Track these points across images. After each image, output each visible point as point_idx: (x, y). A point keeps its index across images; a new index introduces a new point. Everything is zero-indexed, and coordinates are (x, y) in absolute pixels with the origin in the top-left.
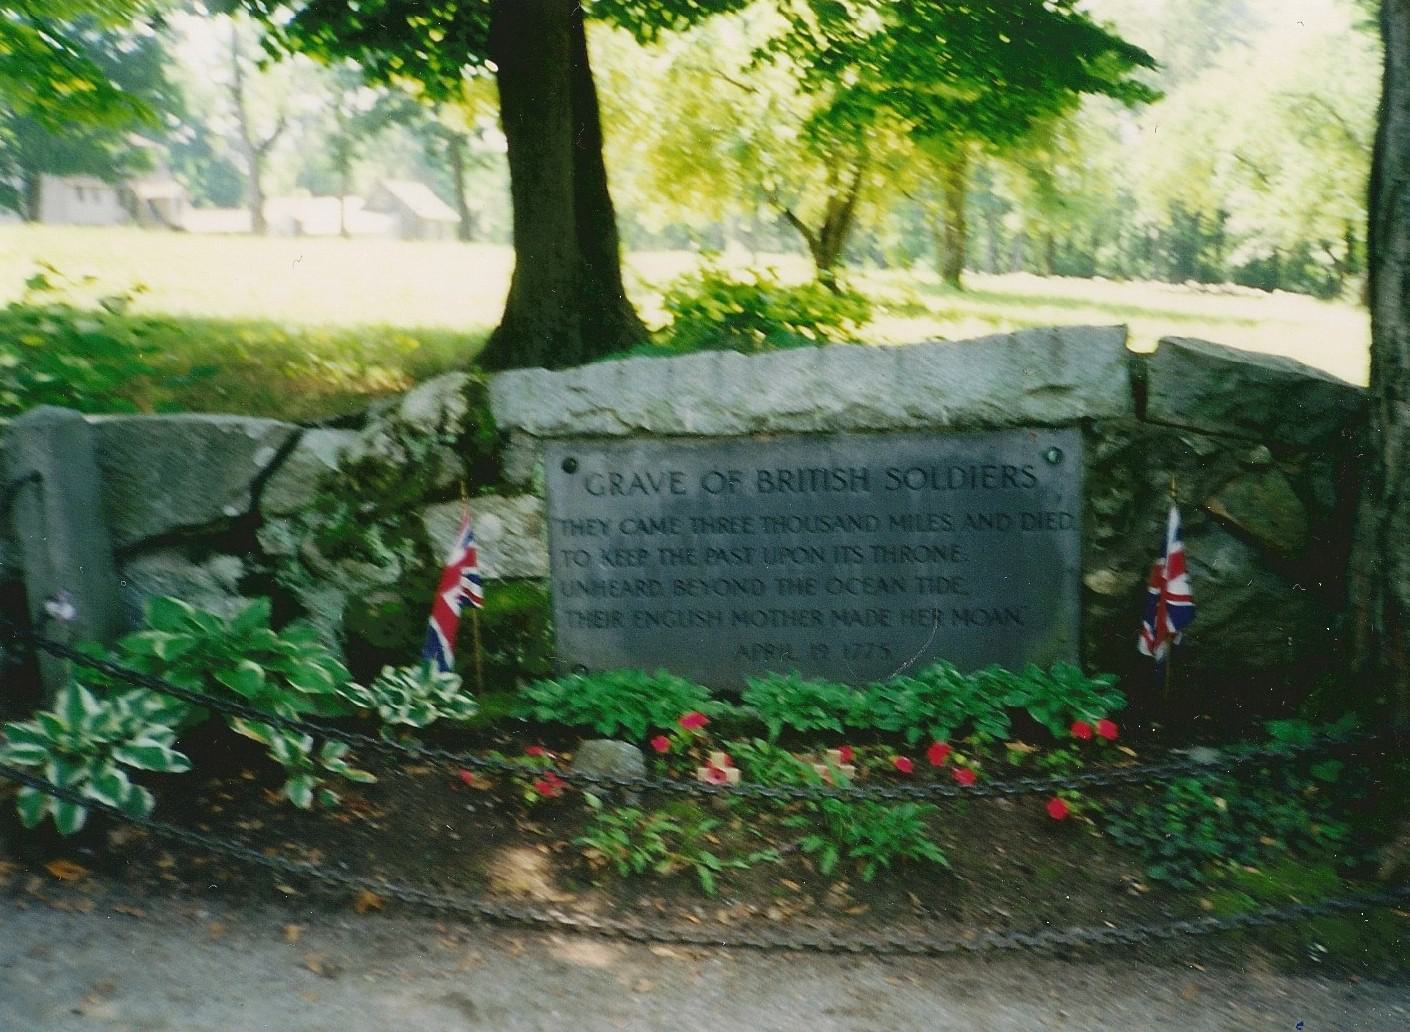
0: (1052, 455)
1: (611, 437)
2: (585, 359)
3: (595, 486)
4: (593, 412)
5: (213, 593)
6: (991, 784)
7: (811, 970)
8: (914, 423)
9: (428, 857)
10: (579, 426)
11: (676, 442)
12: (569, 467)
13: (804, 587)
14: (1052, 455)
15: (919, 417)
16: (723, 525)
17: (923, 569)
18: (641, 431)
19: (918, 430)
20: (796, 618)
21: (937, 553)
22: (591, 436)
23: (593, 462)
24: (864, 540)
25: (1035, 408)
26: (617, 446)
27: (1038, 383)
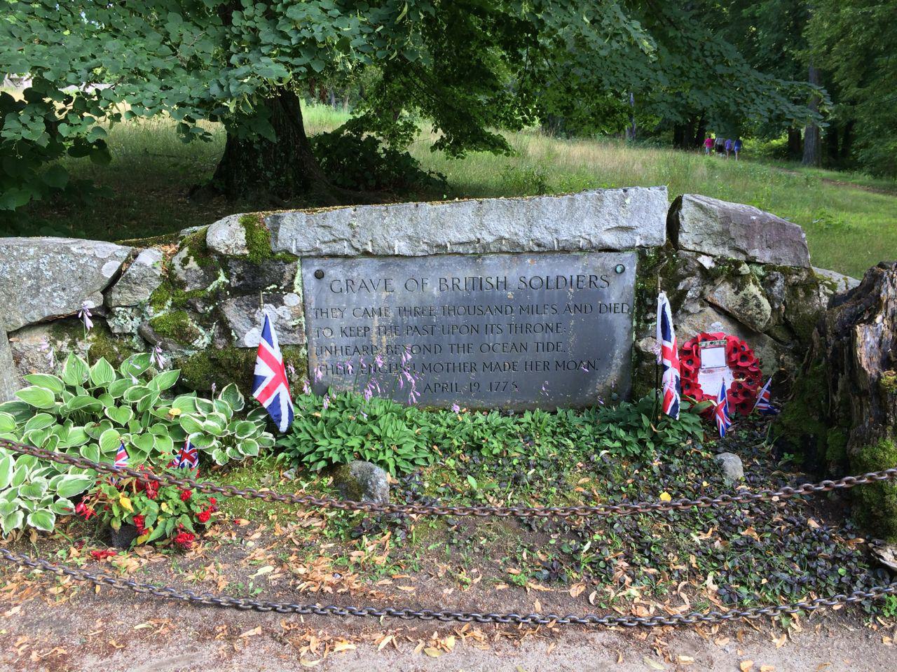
0: (619, 269)
1: (346, 257)
2: (325, 202)
3: (336, 287)
4: (335, 241)
5: (278, 394)
6: (882, 595)
7: (624, 347)
8: (536, 249)
9: (500, 462)
10: (326, 250)
11: (391, 260)
12: (319, 275)
13: (467, 348)
14: (619, 269)
15: (539, 245)
16: (415, 312)
17: (539, 336)
18: (366, 254)
19: (539, 252)
20: (462, 367)
21: (546, 328)
22: (333, 256)
23: (335, 272)
24: (504, 320)
25: (610, 239)
26: (348, 262)
27: (613, 225)
